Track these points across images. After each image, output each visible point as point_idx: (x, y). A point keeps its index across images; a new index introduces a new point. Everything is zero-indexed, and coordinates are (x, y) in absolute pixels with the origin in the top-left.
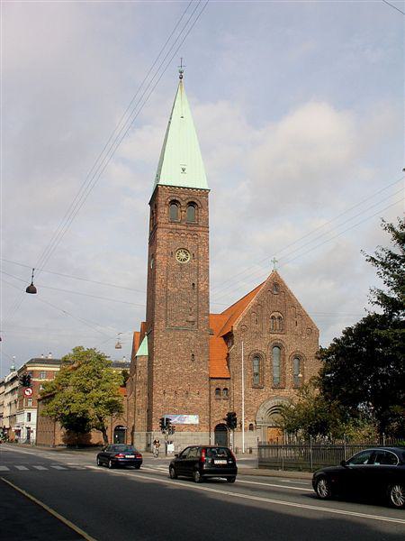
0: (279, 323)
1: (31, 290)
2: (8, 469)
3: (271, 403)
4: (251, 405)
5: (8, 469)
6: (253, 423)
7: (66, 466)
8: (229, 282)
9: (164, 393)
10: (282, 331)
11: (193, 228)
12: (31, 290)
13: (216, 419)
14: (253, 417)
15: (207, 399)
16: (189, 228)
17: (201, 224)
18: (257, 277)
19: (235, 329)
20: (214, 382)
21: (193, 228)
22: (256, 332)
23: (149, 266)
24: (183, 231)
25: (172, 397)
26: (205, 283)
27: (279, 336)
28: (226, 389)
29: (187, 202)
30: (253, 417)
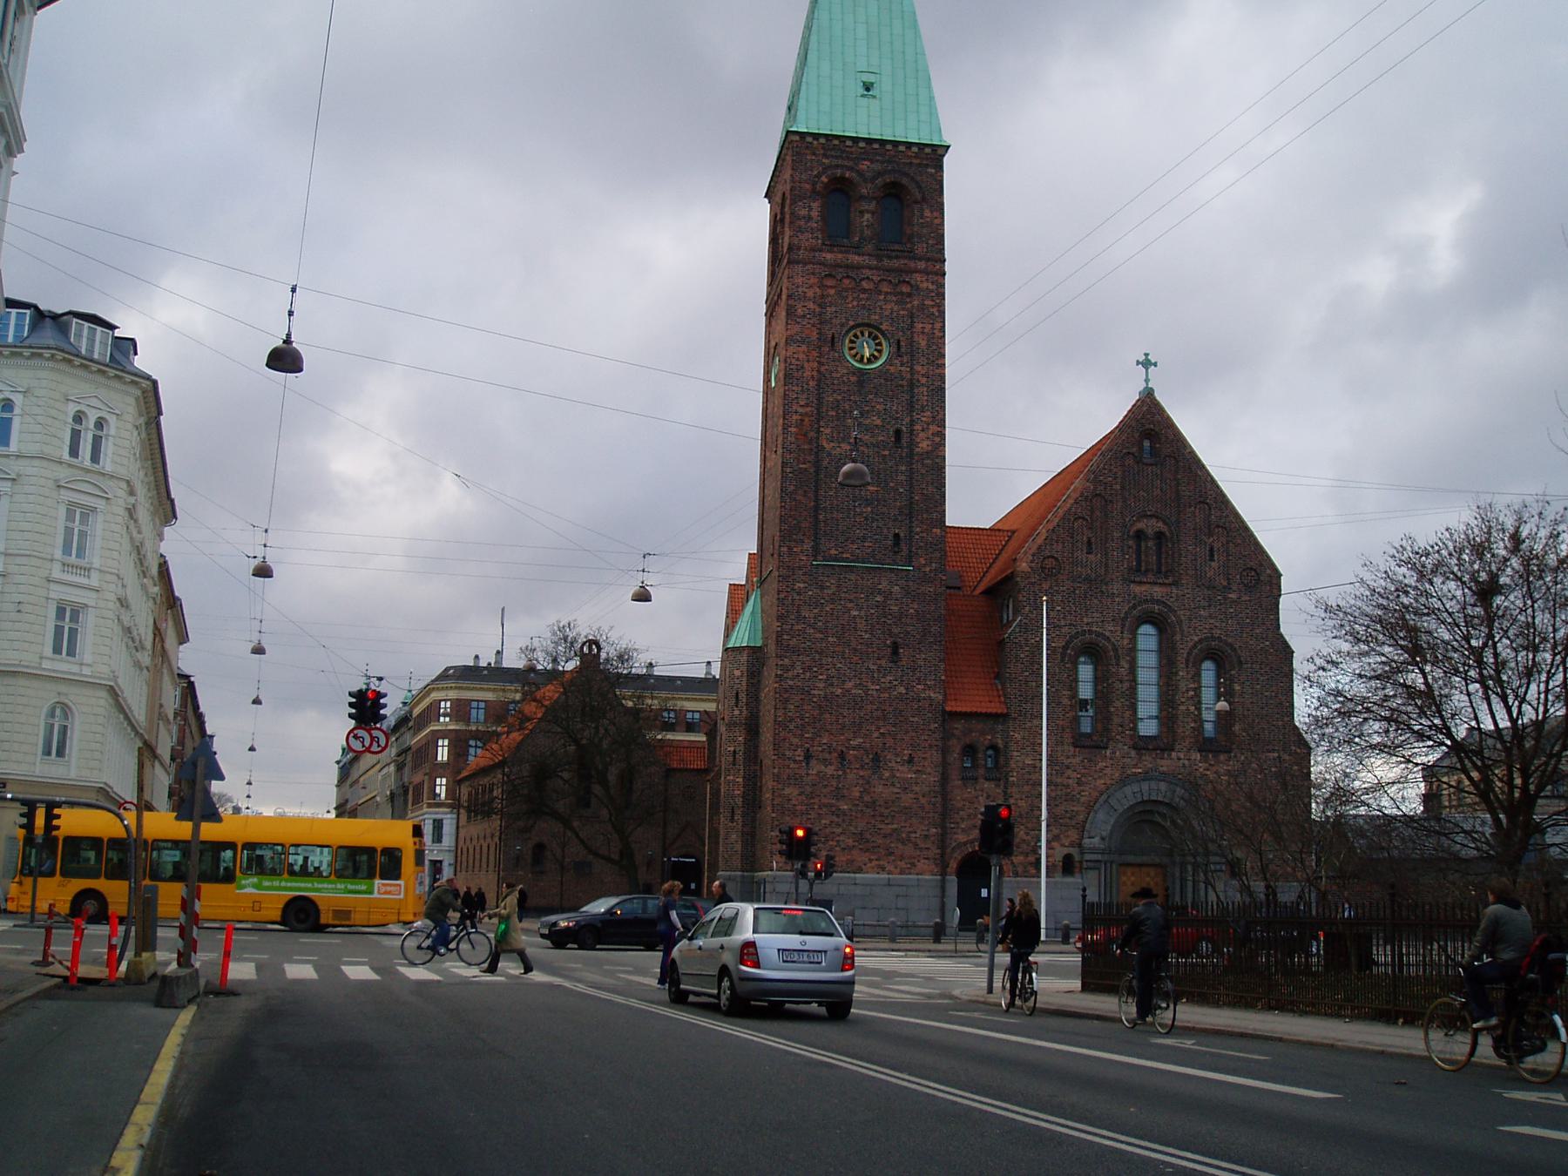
0: (1155, 555)
1: (252, 749)
2: (374, 976)
3: (1128, 796)
4: (1069, 798)
5: (374, 976)
6: (1074, 851)
7: (952, 997)
8: (1006, 445)
9: (808, 757)
10: (1166, 571)
11: (896, 263)
12: (259, 650)
13: (962, 838)
14: (1073, 835)
15: (932, 778)
16: (886, 262)
17: (920, 249)
18: (1088, 418)
19: (1023, 566)
20: (959, 726)
21: (896, 263)
22: (1088, 580)
23: (768, 341)
24: (868, 273)
25: (830, 770)
26: (933, 428)
27: (1158, 592)
28: (994, 747)
29: (879, 181)
30: (1073, 835)
